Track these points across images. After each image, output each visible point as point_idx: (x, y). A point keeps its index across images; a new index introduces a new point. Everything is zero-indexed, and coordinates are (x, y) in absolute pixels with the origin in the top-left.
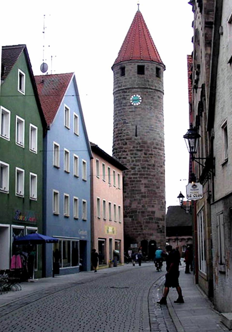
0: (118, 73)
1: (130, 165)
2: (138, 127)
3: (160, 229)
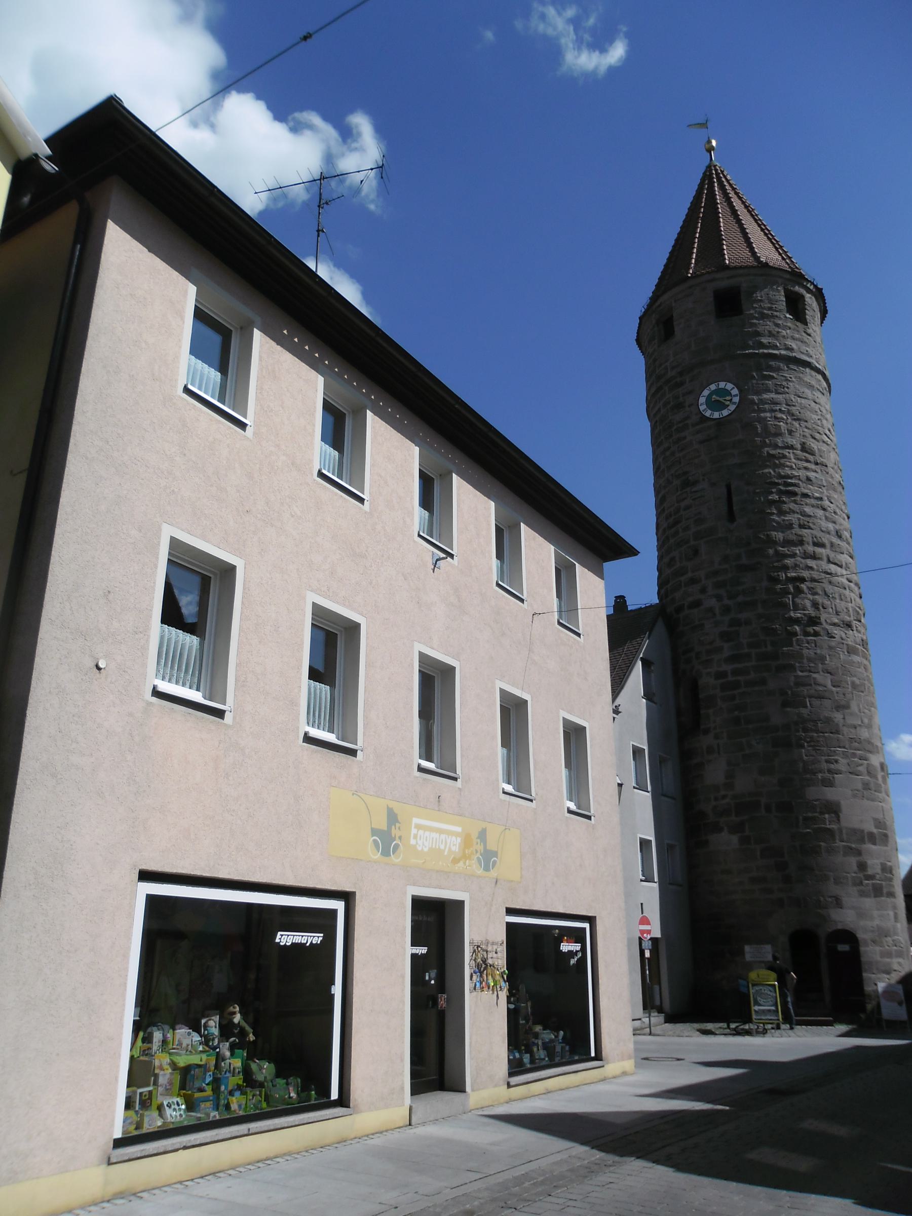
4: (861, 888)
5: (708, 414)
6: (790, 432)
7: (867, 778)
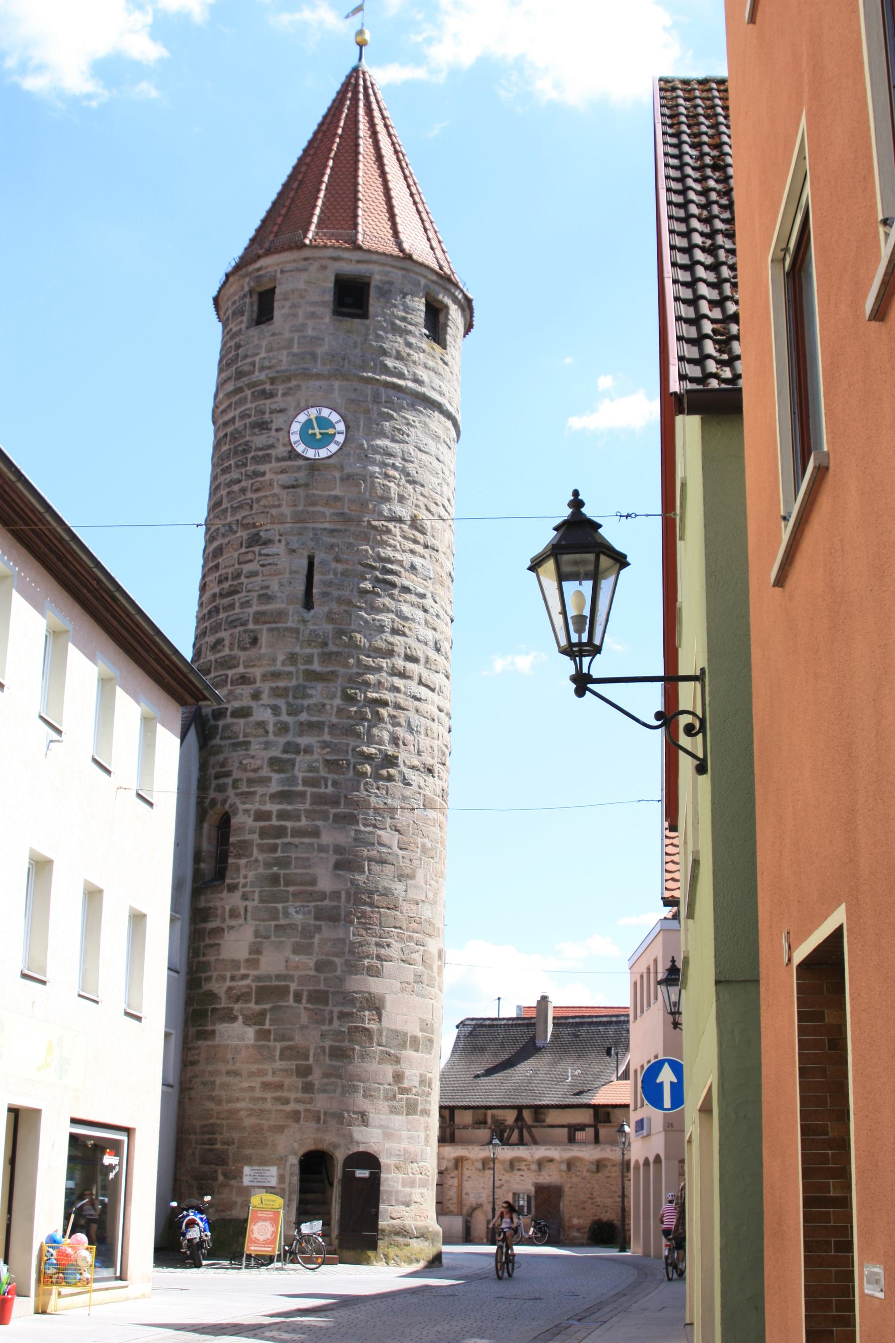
0: (242, 313)
1: (267, 745)
2: (316, 561)
3: (403, 1091)
4: (394, 1103)
5: (300, 448)
7: (421, 968)
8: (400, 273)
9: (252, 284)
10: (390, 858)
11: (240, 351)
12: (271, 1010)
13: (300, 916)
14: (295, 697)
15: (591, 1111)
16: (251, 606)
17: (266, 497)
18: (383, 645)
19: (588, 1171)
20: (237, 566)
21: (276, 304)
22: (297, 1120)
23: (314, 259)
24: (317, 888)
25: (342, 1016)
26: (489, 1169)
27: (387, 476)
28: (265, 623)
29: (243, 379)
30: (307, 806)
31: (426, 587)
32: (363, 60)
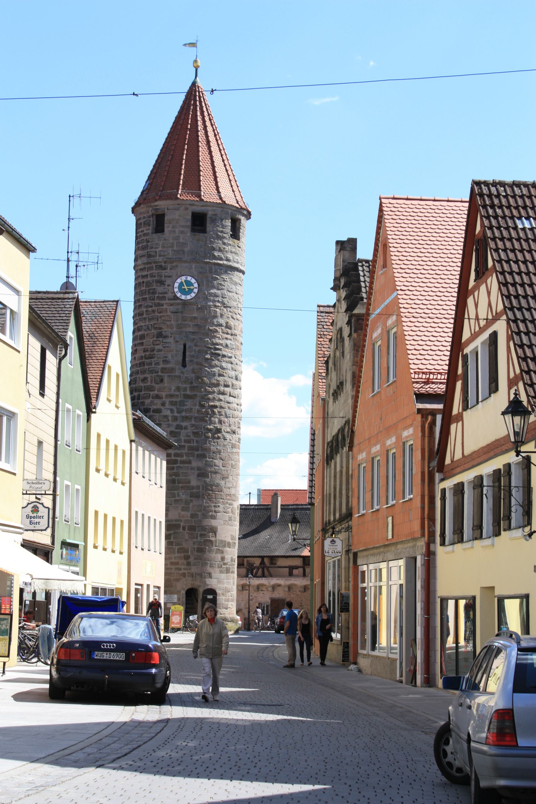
1: (169, 426)
3: (225, 564)
4: (221, 569)
5: (179, 295)
6: (222, 315)
7: (231, 514)
8: (220, 209)
9: (153, 212)
10: (219, 471)
11: (149, 244)
12: (174, 533)
13: (184, 496)
14: (180, 406)
15: (302, 559)
16: (159, 365)
17: (164, 316)
18: (215, 382)
19: (299, 591)
20: (152, 346)
21: (165, 225)
22: (185, 577)
23: (182, 205)
24: (190, 485)
25: (201, 535)
26: (246, 590)
27: (216, 306)
28: (166, 373)
29: (151, 258)
30: (186, 451)
31: (232, 353)
32: (198, 78)
